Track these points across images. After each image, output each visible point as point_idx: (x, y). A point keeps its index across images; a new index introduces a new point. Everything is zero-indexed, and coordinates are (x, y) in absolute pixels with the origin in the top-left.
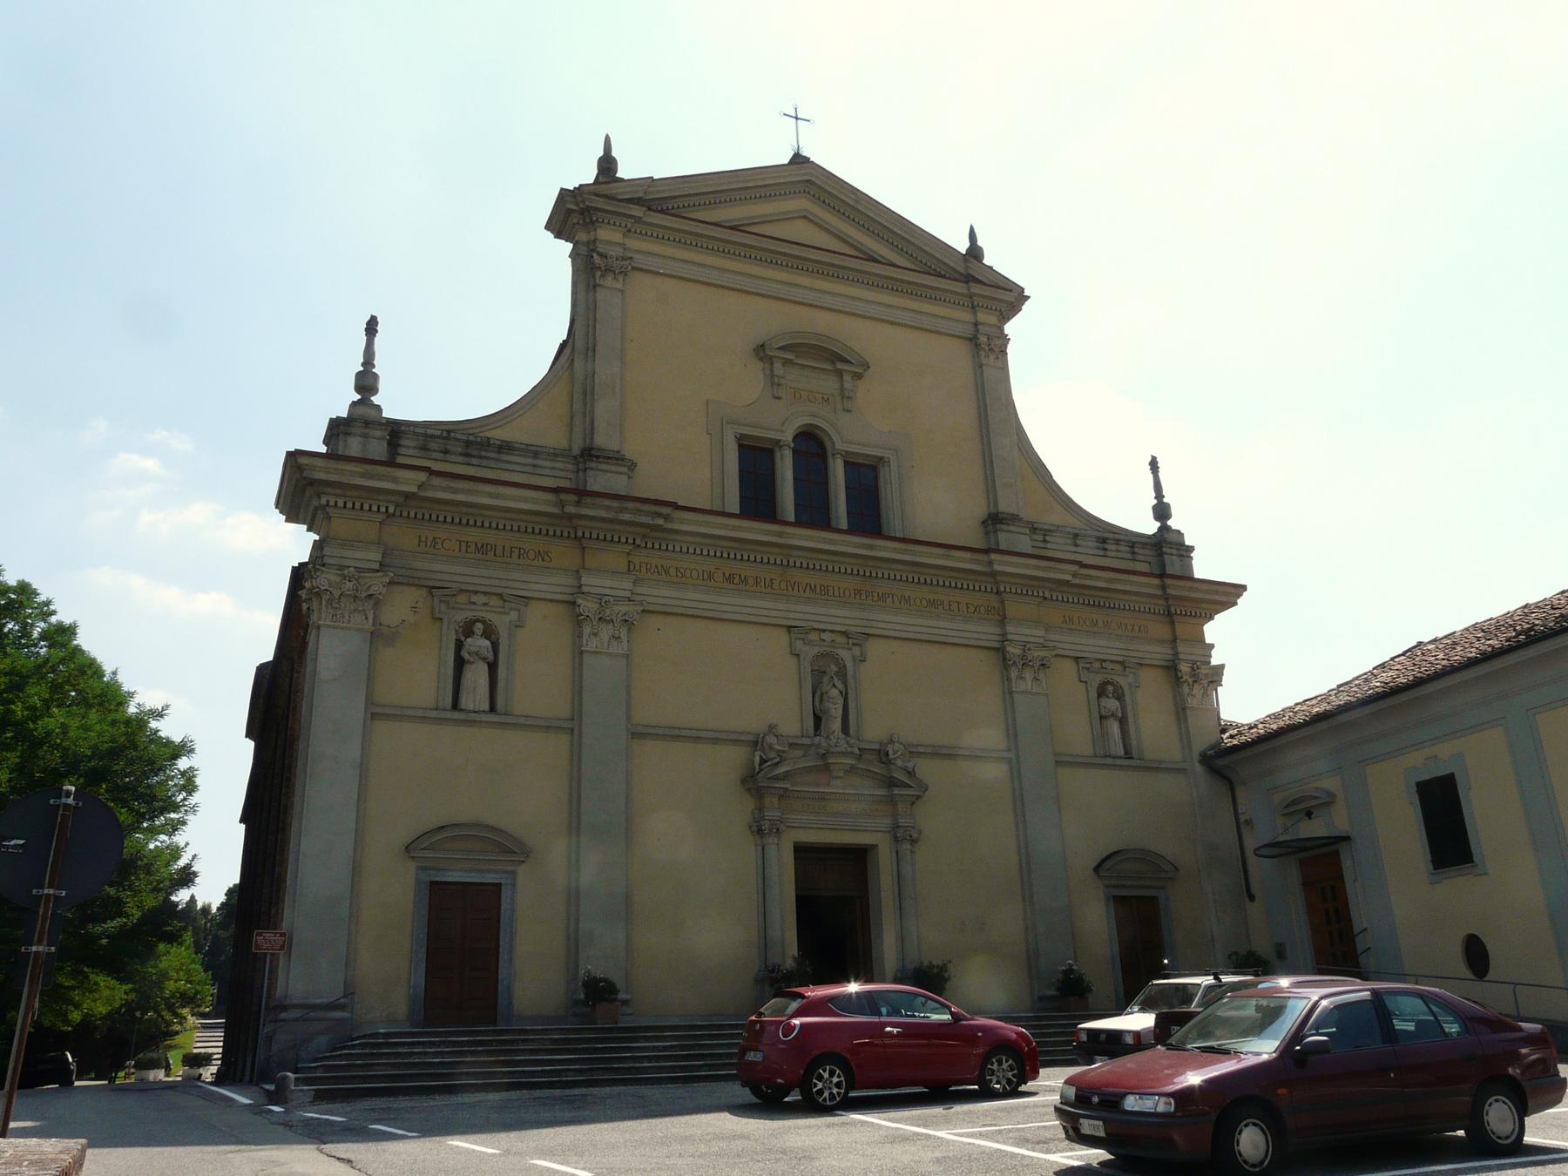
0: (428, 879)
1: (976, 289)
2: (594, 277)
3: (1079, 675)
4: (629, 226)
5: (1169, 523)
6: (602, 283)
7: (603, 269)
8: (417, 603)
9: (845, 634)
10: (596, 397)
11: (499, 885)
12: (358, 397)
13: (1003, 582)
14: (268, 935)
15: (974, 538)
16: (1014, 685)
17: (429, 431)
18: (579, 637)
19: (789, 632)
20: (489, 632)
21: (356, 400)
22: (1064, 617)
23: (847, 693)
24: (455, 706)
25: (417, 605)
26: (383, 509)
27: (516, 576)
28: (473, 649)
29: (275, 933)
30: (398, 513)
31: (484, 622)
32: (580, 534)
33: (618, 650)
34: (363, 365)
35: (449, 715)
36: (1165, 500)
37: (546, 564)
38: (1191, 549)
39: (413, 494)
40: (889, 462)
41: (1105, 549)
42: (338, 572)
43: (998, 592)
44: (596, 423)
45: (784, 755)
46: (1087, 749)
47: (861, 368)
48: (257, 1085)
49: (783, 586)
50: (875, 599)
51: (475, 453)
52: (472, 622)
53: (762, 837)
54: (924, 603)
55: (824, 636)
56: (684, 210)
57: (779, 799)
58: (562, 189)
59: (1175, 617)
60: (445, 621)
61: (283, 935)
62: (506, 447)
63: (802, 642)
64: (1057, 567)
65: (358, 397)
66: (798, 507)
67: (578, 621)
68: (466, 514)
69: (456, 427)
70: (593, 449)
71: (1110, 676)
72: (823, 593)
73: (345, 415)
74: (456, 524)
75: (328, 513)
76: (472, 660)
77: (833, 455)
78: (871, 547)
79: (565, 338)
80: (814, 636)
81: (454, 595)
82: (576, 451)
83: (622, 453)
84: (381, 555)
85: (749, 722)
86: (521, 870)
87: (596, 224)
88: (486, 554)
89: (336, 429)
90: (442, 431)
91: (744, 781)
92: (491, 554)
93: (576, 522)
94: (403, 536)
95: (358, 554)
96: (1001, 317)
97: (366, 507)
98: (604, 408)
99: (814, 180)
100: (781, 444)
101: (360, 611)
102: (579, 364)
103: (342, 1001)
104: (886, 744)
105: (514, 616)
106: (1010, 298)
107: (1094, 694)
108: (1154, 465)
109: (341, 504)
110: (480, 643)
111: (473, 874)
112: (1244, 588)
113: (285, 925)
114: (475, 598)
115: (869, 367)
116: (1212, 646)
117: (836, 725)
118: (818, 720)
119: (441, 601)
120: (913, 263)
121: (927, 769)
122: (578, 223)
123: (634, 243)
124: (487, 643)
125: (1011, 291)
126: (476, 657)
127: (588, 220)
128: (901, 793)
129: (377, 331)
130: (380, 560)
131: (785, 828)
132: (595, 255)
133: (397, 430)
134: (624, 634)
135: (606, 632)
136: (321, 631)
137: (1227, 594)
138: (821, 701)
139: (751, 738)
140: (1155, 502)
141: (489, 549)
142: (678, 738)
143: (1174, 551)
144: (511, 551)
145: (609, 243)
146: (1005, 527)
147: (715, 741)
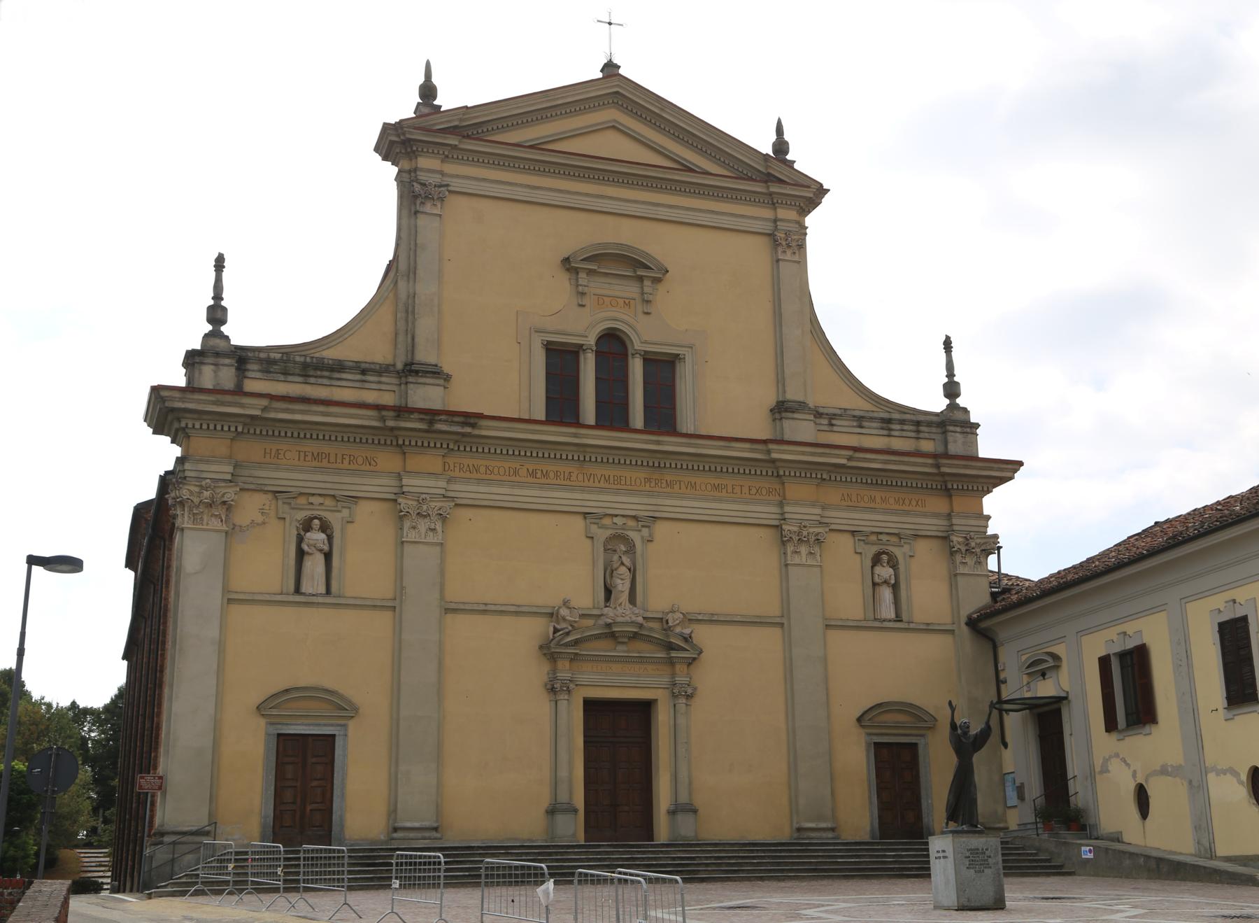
0: (276, 732)
1: (775, 188)
2: (415, 204)
3: (855, 548)
4: (446, 153)
5: (958, 401)
6: (421, 210)
7: (423, 196)
9: (635, 518)
10: (416, 317)
11: (334, 736)
12: (210, 328)
13: (782, 467)
14: (149, 778)
15: (762, 430)
16: (789, 558)
17: (272, 355)
18: (401, 529)
19: (585, 518)
20: (325, 528)
22: (843, 495)
23: (635, 570)
24: (297, 590)
25: (264, 507)
26: (233, 429)
28: (311, 542)
29: (154, 777)
30: (246, 431)
31: (320, 519)
32: (400, 442)
33: (434, 539)
35: (291, 598)
36: (956, 379)
37: (372, 468)
38: (977, 426)
40: (684, 358)
42: (197, 483)
43: (778, 476)
44: (417, 340)
45: (575, 625)
46: (859, 614)
48: (142, 892)
49: (581, 477)
50: (664, 485)
51: (311, 373)
52: (311, 519)
53: (555, 694)
54: (709, 487)
55: (615, 520)
57: (570, 661)
58: (385, 124)
59: (952, 491)
60: (288, 520)
61: (161, 778)
62: (338, 367)
63: (596, 526)
64: (833, 452)
67: (401, 517)
68: (303, 429)
70: (413, 364)
71: (887, 548)
72: (616, 483)
73: (199, 347)
75: (187, 433)
76: (310, 551)
77: (633, 355)
78: (658, 443)
79: (391, 258)
80: (607, 521)
81: (294, 498)
82: (400, 366)
83: (439, 365)
84: (232, 468)
85: (549, 599)
86: (351, 724)
87: (417, 153)
88: (321, 462)
89: (192, 360)
90: (283, 353)
91: (541, 647)
93: (397, 433)
94: (252, 450)
95: (214, 468)
96: (801, 210)
97: (219, 427)
98: (425, 326)
99: (621, 91)
100: (584, 347)
101: (217, 515)
102: (402, 284)
103: (207, 828)
104: (668, 613)
105: (345, 512)
106: (812, 194)
107: (869, 563)
109: (197, 426)
110: (316, 537)
111: (311, 727)
112: (1020, 464)
113: (160, 771)
114: (312, 499)
115: (668, 271)
116: (988, 518)
117: (624, 597)
118: (608, 592)
119: (284, 503)
121: (704, 635)
122: (401, 152)
123: (450, 168)
124: (323, 536)
126: (313, 548)
127: (409, 150)
128: (681, 656)
130: (232, 472)
131: (574, 687)
132: (415, 184)
133: (243, 357)
134: (439, 528)
135: (423, 525)
136: (185, 534)
137: (1005, 470)
138: (612, 576)
139: (549, 611)
140: (946, 380)
142: (484, 612)
143: (958, 429)
144: (750, 490)
145: (429, 171)
146: (790, 415)
147: (517, 613)
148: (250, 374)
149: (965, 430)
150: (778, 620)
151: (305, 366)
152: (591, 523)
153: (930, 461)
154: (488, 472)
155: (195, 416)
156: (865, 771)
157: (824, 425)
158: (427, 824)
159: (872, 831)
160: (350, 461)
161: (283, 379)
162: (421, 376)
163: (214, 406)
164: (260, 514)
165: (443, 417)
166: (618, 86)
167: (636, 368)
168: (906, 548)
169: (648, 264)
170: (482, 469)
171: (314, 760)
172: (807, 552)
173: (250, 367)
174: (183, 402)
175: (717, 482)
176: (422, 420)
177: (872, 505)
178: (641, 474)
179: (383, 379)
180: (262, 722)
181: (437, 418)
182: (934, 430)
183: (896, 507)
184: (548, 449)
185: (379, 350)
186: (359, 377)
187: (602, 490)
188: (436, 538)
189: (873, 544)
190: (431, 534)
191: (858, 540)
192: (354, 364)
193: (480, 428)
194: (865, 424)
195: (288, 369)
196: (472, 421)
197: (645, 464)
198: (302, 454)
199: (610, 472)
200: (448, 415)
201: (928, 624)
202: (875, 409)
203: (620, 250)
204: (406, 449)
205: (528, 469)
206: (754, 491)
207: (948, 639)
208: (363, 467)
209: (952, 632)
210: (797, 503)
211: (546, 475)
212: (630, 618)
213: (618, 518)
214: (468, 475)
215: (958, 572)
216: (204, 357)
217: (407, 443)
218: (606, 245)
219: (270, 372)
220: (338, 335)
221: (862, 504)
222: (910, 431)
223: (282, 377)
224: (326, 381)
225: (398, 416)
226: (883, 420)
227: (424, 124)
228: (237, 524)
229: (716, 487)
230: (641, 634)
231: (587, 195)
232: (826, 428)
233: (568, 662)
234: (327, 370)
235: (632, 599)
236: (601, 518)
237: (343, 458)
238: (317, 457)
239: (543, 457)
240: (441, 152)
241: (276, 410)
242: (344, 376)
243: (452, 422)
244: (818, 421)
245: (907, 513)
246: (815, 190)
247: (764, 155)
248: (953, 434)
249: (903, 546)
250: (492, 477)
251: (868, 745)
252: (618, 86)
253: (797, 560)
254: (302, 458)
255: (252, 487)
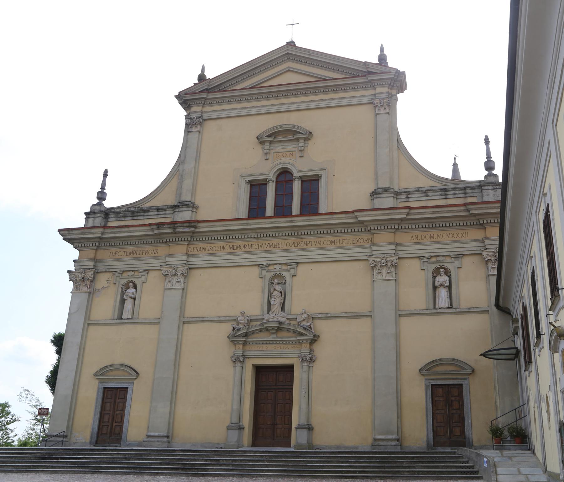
1: (371, 78)
4: (389, 83)
5: (104, 202)
8: (109, 278)
9: (286, 264)
11: (127, 388)
12: (487, 173)
17: (122, 210)
20: (447, 273)
21: (486, 174)
22: (415, 236)
27: (143, 262)
30: (400, 228)
34: (487, 158)
37: (155, 255)
39: (405, 218)
41: (446, 195)
43: (480, 224)
47: (309, 136)
49: (257, 246)
55: (275, 267)
56: (230, 87)
62: (149, 209)
65: (487, 173)
66: (302, 205)
68: (124, 241)
69: (132, 205)
74: (129, 245)
80: (434, 259)
81: (430, 259)
85: (235, 312)
90: (126, 208)
92: (135, 255)
95: (86, 264)
107: (430, 275)
108: (105, 174)
110: (131, 291)
111: (118, 384)
114: (438, 258)
120: (345, 75)
121: (321, 327)
125: (390, 72)
129: (489, 142)
133: (107, 213)
141: (135, 253)
142: (203, 322)
143: (491, 187)
144: (353, 241)
147: (219, 321)
148: (110, 220)
149: (495, 187)
150: (368, 314)
151: (133, 212)
152: (262, 270)
153: (462, 208)
154: (210, 250)
155: (78, 241)
156: (424, 403)
157: (403, 198)
158: (161, 434)
159: (428, 441)
160: (146, 252)
161: (124, 220)
162: (181, 208)
163: (82, 235)
164: (107, 283)
165: (179, 225)
166: (288, 50)
167: (297, 186)
168: (457, 264)
169: (300, 131)
170: (207, 249)
171: (119, 400)
172: (386, 272)
173: (110, 216)
174: (70, 235)
175: (333, 239)
176: (170, 227)
177: (432, 240)
178: (289, 241)
179: (167, 212)
180: (97, 382)
181: (176, 226)
182: (476, 191)
183: (448, 239)
184: (361, 227)
185: (169, 199)
186: (156, 213)
187: (267, 252)
188: (180, 286)
189: (433, 263)
190: (178, 284)
191: (423, 262)
192: (156, 207)
193: (199, 227)
194: (430, 194)
195: (126, 214)
196: (193, 224)
197: (290, 234)
198: (126, 252)
199: (273, 241)
200: (181, 223)
201: (469, 308)
202: (440, 185)
203: (283, 128)
204: (373, 232)
205: (230, 246)
206: (356, 241)
207: (485, 316)
208: (152, 255)
209: (486, 312)
210: (379, 245)
211: (239, 247)
212: (278, 319)
213: (277, 265)
214: (200, 252)
215: (490, 274)
216: (90, 215)
217: (372, 228)
218: (278, 127)
219: (118, 217)
220: (151, 196)
221: (425, 240)
222: (460, 194)
223: (123, 219)
224: (141, 217)
225: (158, 227)
226: (441, 190)
227: (192, 91)
228: (97, 288)
229: (333, 242)
230: (249, 332)
231: (272, 105)
232: (405, 200)
233: (308, 344)
234: (142, 212)
235: (283, 309)
236: (268, 267)
237: (143, 252)
238: (132, 253)
239: (405, 228)
240: (200, 102)
241: (108, 233)
242: (150, 214)
243: (184, 226)
244: (399, 197)
245: (454, 242)
246: (394, 73)
247: (364, 63)
248: (486, 191)
249: (454, 262)
250: (212, 252)
251: (427, 386)
252: (288, 50)
253: (380, 277)
254: (125, 254)
255: (104, 270)
